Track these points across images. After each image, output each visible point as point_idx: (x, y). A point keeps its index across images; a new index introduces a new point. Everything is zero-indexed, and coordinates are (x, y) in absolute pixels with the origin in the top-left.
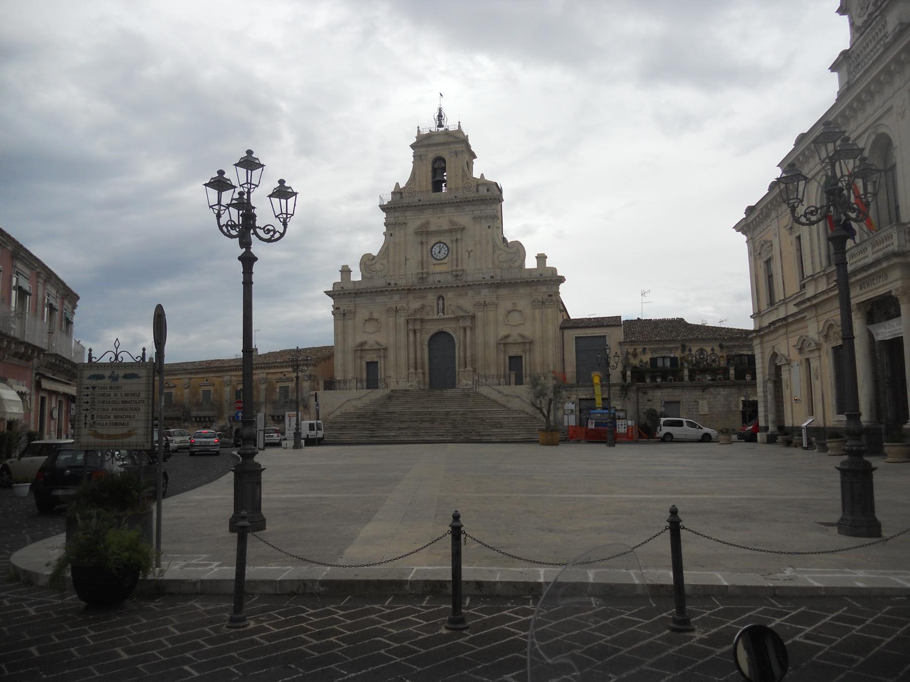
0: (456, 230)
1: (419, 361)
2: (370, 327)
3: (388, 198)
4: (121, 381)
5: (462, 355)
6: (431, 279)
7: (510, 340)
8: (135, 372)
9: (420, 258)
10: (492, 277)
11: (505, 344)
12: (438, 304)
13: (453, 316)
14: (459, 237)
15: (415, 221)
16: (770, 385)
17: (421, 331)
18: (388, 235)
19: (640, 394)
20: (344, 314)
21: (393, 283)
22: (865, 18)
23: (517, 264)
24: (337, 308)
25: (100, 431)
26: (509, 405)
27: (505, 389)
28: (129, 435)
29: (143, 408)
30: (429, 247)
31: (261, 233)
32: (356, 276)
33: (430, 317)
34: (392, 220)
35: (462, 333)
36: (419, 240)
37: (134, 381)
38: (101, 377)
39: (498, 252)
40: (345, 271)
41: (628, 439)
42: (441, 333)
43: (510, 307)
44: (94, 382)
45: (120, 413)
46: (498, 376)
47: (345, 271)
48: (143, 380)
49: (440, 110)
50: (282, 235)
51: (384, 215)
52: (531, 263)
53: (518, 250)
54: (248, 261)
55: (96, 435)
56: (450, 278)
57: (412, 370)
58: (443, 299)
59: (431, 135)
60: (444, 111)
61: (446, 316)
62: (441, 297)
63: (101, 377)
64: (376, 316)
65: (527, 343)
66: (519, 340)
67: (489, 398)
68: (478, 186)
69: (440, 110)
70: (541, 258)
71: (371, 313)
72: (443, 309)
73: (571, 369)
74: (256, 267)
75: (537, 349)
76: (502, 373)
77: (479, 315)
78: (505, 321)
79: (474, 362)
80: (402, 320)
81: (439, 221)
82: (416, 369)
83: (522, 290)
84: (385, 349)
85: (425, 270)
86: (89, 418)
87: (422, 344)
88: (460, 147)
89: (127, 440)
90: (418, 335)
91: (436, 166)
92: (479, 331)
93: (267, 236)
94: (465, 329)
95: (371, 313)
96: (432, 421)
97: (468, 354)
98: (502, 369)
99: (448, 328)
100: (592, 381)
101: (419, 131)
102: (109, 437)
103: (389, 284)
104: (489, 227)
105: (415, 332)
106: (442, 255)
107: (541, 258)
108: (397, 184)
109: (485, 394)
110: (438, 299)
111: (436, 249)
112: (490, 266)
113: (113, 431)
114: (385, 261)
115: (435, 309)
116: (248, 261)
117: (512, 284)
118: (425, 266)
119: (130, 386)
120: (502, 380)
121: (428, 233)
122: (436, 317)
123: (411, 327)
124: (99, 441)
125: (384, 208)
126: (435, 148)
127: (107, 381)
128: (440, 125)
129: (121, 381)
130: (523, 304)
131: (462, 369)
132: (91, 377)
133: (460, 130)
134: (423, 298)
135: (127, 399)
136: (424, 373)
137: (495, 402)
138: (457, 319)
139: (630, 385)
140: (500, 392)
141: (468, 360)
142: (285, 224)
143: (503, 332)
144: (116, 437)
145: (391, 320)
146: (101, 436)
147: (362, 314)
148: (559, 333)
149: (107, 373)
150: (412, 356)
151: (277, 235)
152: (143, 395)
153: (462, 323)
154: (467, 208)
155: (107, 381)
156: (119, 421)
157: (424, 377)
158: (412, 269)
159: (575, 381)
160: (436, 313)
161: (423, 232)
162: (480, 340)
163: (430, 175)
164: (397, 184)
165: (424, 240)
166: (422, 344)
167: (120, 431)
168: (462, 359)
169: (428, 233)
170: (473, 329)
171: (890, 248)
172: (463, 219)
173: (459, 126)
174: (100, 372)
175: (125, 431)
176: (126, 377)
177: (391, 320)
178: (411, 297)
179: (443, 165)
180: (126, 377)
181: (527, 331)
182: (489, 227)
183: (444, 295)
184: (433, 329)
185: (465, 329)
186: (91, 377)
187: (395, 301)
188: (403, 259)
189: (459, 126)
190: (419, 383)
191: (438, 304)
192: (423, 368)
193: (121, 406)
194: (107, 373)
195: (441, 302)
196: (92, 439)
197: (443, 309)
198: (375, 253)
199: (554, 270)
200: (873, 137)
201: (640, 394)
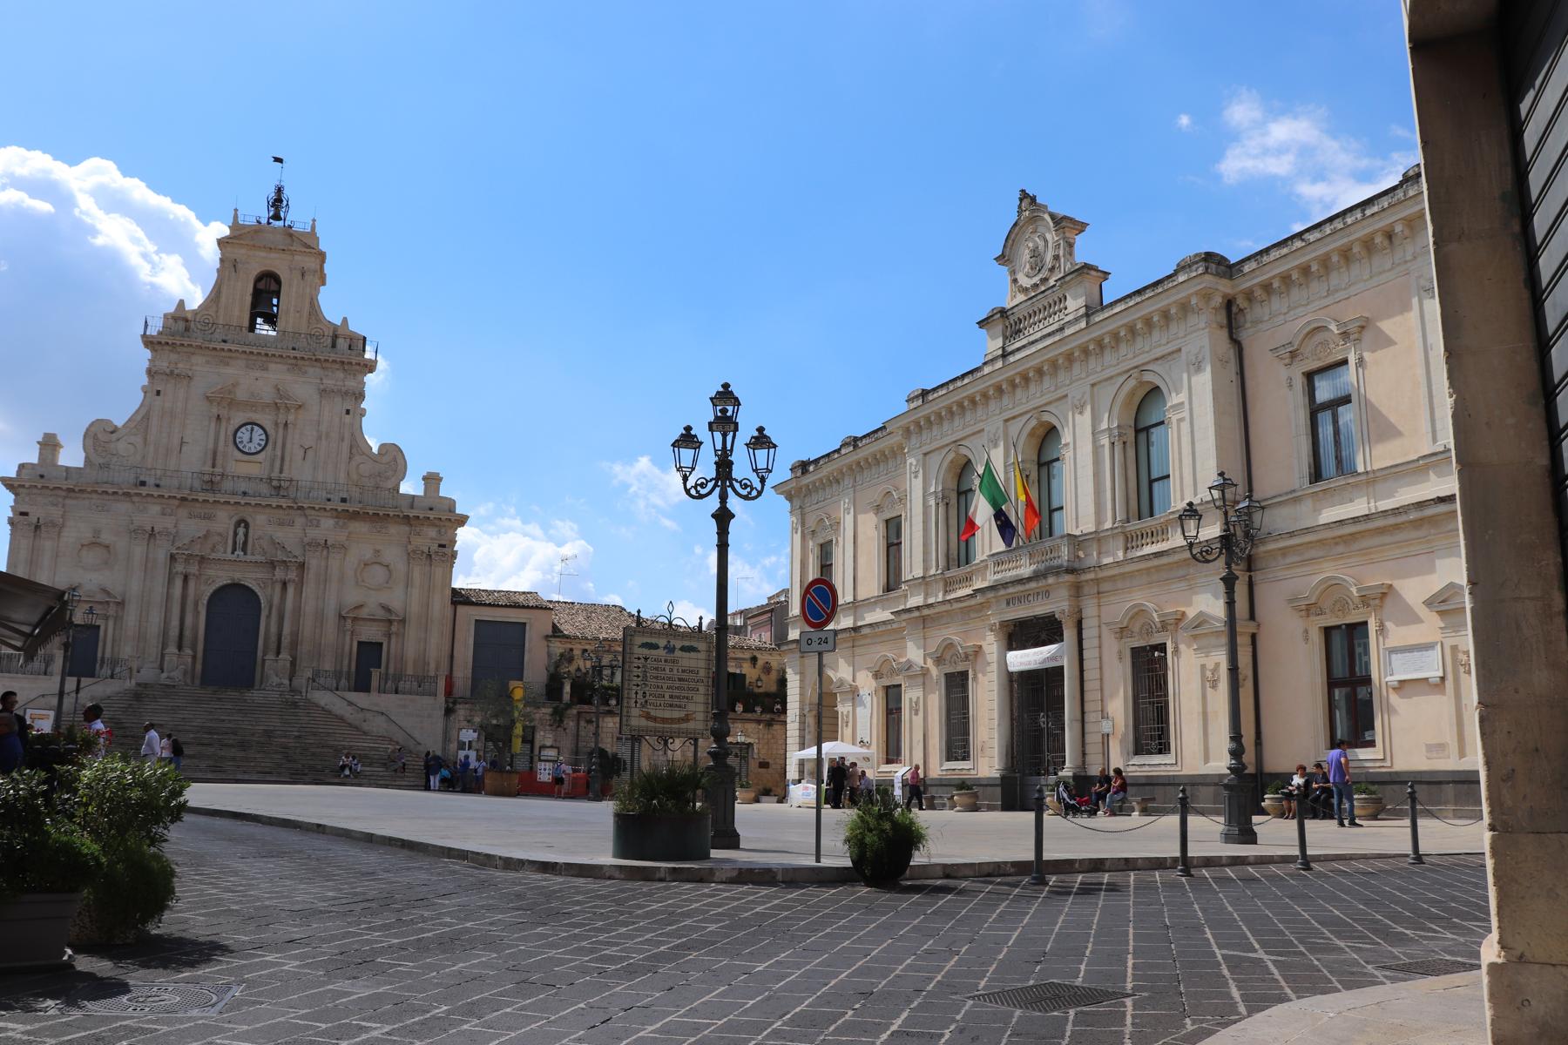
0: (282, 404)
1: (188, 633)
2: (90, 557)
3: (155, 328)
4: (678, 653)
5: (274, 629)
6: (227, 485)
7: (364, 613)
8: (695, 644)
9: (211, 446)
10: (344, 500)
11: (355, 619)
12: (236, 534)
13: (262, 559)
14: (291, 418)
15: (207, 374)
16: (811, 721)
17: (198, 577)
18: (153, 393)
19: (582, 723)
20: (37, 527)
21: (151, 481)
22: (1036, 280)
23: (390, 485)
24: (23, 514)
25: (653, 713)
26: (366, 727)
27: (360, 698)
28: (686, 719)
29: (702, 690)
30: (231, 429)
31: (737, 486)
32: (72, 456)
33: (219, 555)
34: (163, 365)
35: (278, 588)
36: (215, 411)
37: (693, 655)
38: (655, 647)
39: (358, 459)
40: (49, 444)
41: (552, 790)
42: (236, 588)
43: (368, 554)
44: (646, 651)
45: (676, 692)
46: (338, 675)
47: (49, 444)
48: (702, 655)
49: (279, 190)
50: (760, 493)
51: (147, 354)
52: (410, 486)
53: (395, 459)
54: (723, 518)
55: (648, 717)
56: (264, 489)
57: (172, 649)
58: (247, 526)
59: (258, 229)
60: (286, 193)
61: (249, 558)
62: (243, 522)
63: (655, 647)
64: (106, 538)
65: (392, 620)
66: (381, 614)
67: (330, 712)
68: (335, 337)
69: (279, 190)
70: (432, 480)
71: (97, 533)
72: (245, 543)
73: (463, 672)
74: (733, 526)
75: (412, 633)
76: (345, 669)
77: (314, 562)
78: (351, 581)
79: (295, 644)
80: (161, 555)
81: (258, 383)
82: (180, 647)
83: (395, 530)
84: (121, 604)
85: (218, 470)
86: (640, 695)
87: (196, 604)
88: (310, 263)
89: (684, 726)
90: (192, 584)
91: (261, 285)
92: (309, 590)
93: (744, 492)
94: (284, 584)
95: (97, 533)
96: (243, 745)
97: (286, 630)
98: (346, 662)
99: (251, 579)
100: (509, 696)
101: (236, 217)
102: (664, 720)
103: (143, 484)
104: (348, 412)
105: (186, 578)
106: (253, 447)
107: (432, 480)
108: (181, 303)
109: (322, 703)
110: (238, 524)
111: (244, 435)
112: (342, 478)
113: (667, 714)
114: (138, 440)
115: (230, 542)
116: (723, 518)
117: (378, 518)
118: (219, 462)
119: (688, 660)
120: (343, 682)
121: (233, 404)
122: (229, 556)
123: (179, 568)
124: (651, 724)
125: (148, 342)
126: (263, 254)
127: (661, 652)
128: (277, 217)
129: (678, 653)
130: (393, 555)
131: (271, 656)
132: (644, 645)
133: (313, 233)
134: (208, 517)
135: (684, 676)
136: (194, 657)
137: (341, 719)
138: (272, 565)
139: (568, 706)
140: (350, 703)
141: (286, 641)
142: (763, 480)
143: (352, 597)
144: (672, 721)
145: (139, 551)
146: (655, 719)
147: (77, 529)
148: (449, 609)
149: (662, 642)
150: (175, 623)
151: (754, 493)
152: (702, 673)
153: (279, 574)
154: (311, 370)
155: (661, 652)
156: (676, 702)
157: (194, 663)
158: (192, 461)
159: (468, 694)
160: (229, 549)
161: (224, 400)
162: (309, 607)
163: (249, 299)
164: (181, 303)
165: (224, 413)
166: (196, 604)
167: (677, 714)
168: (273, 638)
169: (233, 404)
170: (300, 584)
171: (1056, 563)
172: (302, 387)
173: (313, 227)
174: (654, 641)
175: (682, 714)
176: (683, 649)
177: (139, 551)
178: (183, 512)
179: (274, 287)
180: (683, 649)
181: (395, 599)
182: (348, 412)
183: (249, 520)
184: (222, 577)
185: (284, 584)
186: (644, 645)
187: (152, 515)
188: (176, 442)
189: (313, 227)
190: (185, 673)
191: (236, 534)
192: (194, 648)
193: (677, 684)
194: (662, 642)
195: (241, 531)
196: (644, 722)
197: (245, 543)
198: (119, 422)
199: (451, 504)
200: (1034, 423)
201: (582, 723)
